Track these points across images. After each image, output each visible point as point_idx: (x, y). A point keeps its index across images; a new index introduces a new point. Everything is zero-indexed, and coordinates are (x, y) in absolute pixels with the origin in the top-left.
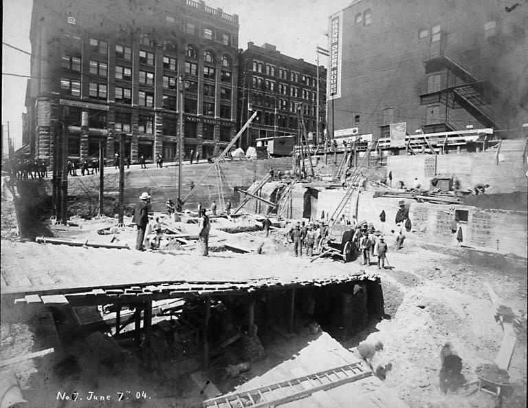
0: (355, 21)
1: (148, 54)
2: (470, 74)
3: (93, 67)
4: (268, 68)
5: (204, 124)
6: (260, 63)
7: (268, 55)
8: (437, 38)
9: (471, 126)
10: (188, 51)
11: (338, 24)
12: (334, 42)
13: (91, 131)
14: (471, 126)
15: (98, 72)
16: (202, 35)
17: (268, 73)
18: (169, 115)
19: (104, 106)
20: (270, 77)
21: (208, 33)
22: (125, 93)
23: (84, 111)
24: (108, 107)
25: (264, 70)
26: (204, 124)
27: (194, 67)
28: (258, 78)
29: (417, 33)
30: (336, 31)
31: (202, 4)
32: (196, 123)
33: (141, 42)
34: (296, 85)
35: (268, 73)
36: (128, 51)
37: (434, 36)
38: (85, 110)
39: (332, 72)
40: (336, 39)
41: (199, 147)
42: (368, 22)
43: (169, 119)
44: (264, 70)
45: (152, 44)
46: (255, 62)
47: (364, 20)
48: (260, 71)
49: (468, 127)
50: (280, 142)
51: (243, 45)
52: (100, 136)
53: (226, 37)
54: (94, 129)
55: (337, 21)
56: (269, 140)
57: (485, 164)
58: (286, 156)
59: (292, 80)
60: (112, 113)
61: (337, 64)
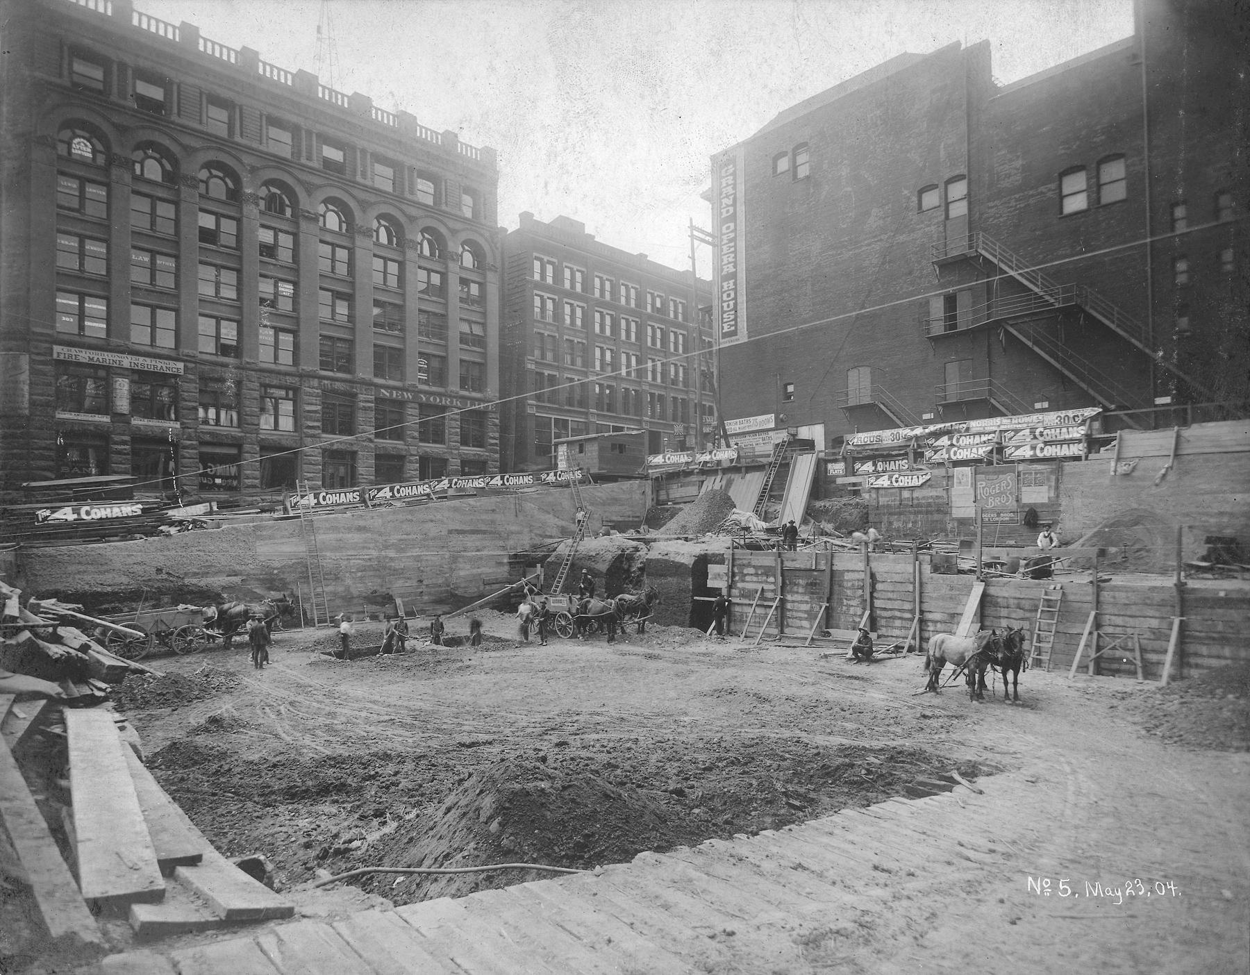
0: (775, 168)
1: (223, 220)
2: (1036, 290)
3: (140, 265)
4: (567, 273)
5: (421, 406)
6: (549, 262)
7: (565, 245)
8: (959, 210)
9: (1046, 405)
10: (421, 244)
11: (734, 174)
12: (725, 215)
13: (138, 428)
14: (1046, 405)
15: (82, 264)
16: (412, 192)
17: (567, 285)
18: (338, 385)
19: (172, 364)
20: (571, 294)
21: (425, 189)
22: (223, 331)
23: (123, 376)
24: (181, 365)
25: (558, 276)
26: (421, 406)
27: (393, 268)
28: (546, 295)
29: (915, 199)
30: (730, 190)
31: (124, 11)
32: (401, 404)
33: (321, 223)
34: (679, 326)
35: (567, 285)
36: (228, 227)
37: (951, 207)
38: (123, 372)
39: (725, 284)
40: (731, 209)
41: (410, 462)
42: (803, 172)
43: (335, 392)
44: (558, 276)
45: (344, 226)
46: (537, 258)
47: (795, 167)
48: (549, 280)
49: (1038, 406)
50: (614, 447)
51: (508, 219)
52: (161, 439)
53: (467, 200)
54: (145, 422)
55: (731, 169)
56: (586, 440)
57: (273, 793)
58: (630, 478)
59: (623, 300)
60: (191, 381)
61: (735, 267)
